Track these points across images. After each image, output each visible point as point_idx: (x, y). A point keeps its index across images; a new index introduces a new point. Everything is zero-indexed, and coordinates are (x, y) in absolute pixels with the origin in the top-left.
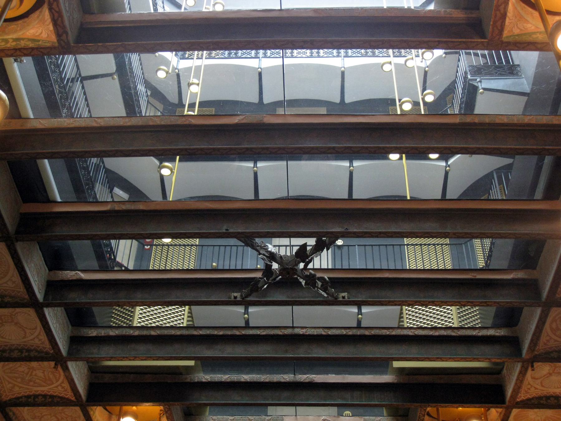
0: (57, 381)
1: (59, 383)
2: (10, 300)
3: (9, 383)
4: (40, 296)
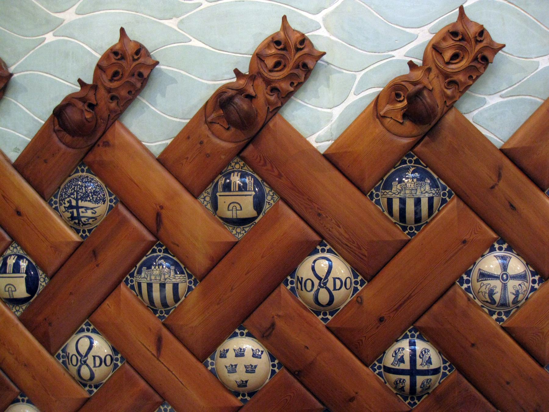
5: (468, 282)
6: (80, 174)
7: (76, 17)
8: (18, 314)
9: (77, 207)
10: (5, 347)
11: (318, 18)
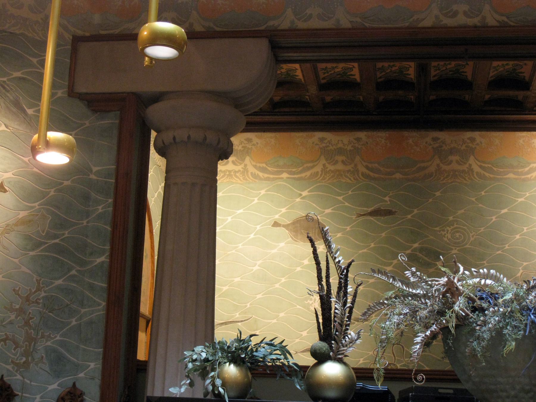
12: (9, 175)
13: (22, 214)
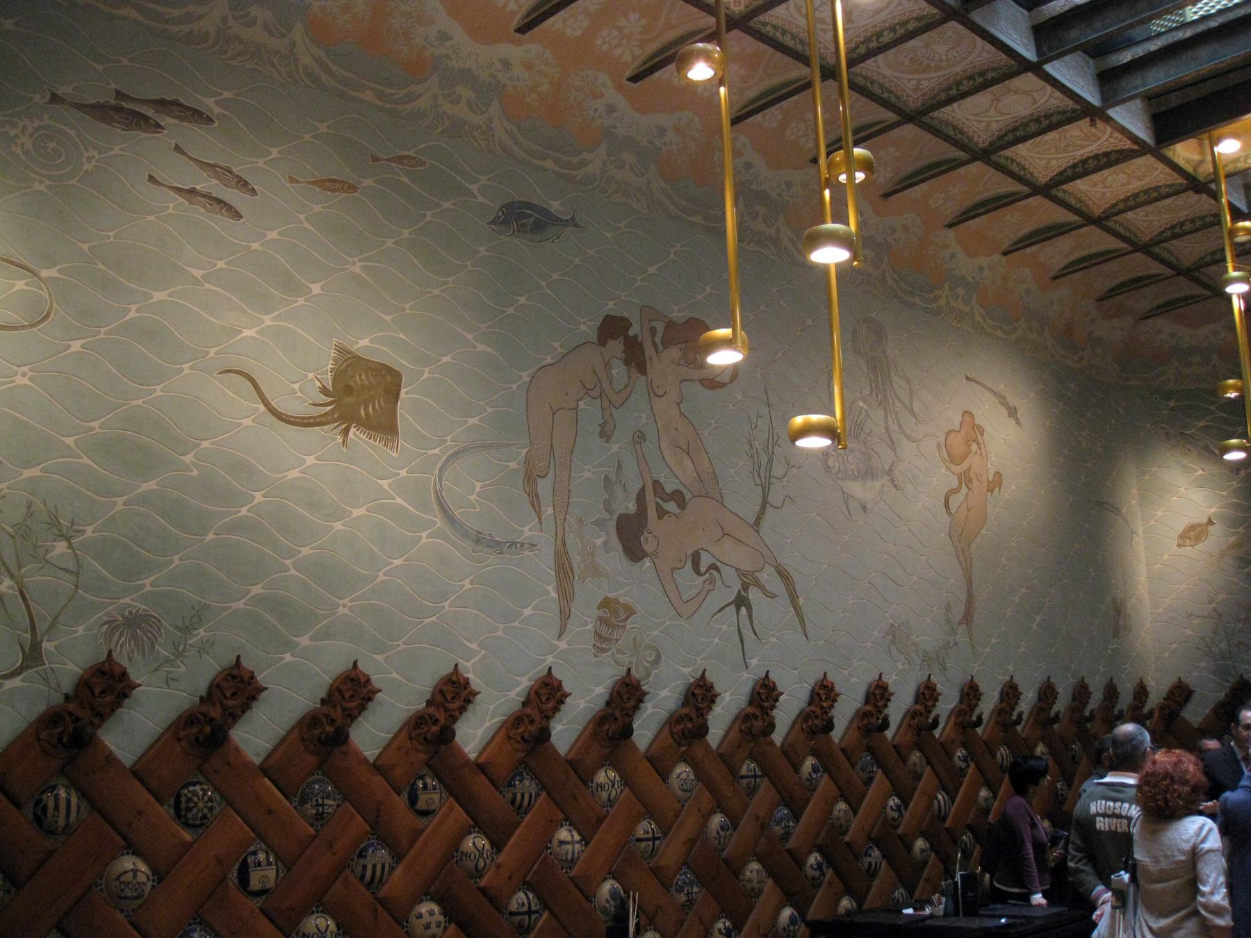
0: (1105, 133)
1: (1106, 136)
2: (994, 74)
3: (1040, 159)
4: (1030, 54)
5: (550, 848)
6: (316, 776)
7: (309, 643)
8: (259, 905)
9: (323, 805)
10: (730, 798)
11: (469, 665)
12: (1213, 510)
13: (1232, 539)
